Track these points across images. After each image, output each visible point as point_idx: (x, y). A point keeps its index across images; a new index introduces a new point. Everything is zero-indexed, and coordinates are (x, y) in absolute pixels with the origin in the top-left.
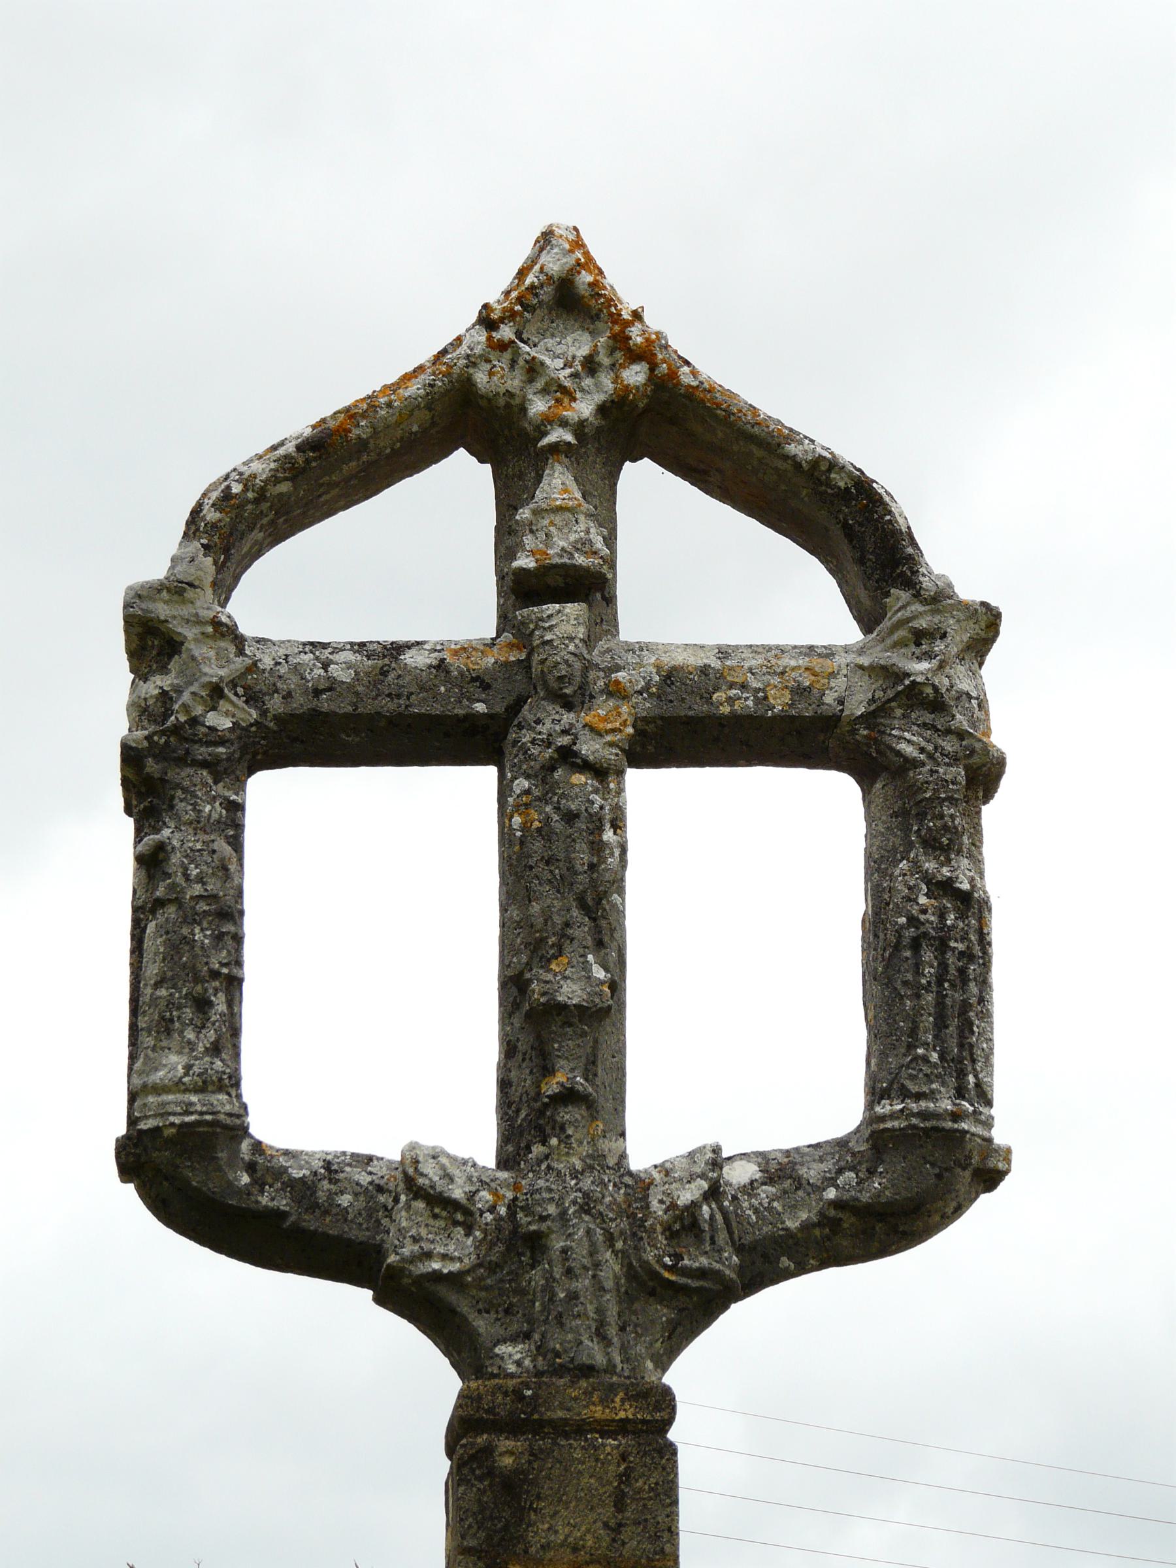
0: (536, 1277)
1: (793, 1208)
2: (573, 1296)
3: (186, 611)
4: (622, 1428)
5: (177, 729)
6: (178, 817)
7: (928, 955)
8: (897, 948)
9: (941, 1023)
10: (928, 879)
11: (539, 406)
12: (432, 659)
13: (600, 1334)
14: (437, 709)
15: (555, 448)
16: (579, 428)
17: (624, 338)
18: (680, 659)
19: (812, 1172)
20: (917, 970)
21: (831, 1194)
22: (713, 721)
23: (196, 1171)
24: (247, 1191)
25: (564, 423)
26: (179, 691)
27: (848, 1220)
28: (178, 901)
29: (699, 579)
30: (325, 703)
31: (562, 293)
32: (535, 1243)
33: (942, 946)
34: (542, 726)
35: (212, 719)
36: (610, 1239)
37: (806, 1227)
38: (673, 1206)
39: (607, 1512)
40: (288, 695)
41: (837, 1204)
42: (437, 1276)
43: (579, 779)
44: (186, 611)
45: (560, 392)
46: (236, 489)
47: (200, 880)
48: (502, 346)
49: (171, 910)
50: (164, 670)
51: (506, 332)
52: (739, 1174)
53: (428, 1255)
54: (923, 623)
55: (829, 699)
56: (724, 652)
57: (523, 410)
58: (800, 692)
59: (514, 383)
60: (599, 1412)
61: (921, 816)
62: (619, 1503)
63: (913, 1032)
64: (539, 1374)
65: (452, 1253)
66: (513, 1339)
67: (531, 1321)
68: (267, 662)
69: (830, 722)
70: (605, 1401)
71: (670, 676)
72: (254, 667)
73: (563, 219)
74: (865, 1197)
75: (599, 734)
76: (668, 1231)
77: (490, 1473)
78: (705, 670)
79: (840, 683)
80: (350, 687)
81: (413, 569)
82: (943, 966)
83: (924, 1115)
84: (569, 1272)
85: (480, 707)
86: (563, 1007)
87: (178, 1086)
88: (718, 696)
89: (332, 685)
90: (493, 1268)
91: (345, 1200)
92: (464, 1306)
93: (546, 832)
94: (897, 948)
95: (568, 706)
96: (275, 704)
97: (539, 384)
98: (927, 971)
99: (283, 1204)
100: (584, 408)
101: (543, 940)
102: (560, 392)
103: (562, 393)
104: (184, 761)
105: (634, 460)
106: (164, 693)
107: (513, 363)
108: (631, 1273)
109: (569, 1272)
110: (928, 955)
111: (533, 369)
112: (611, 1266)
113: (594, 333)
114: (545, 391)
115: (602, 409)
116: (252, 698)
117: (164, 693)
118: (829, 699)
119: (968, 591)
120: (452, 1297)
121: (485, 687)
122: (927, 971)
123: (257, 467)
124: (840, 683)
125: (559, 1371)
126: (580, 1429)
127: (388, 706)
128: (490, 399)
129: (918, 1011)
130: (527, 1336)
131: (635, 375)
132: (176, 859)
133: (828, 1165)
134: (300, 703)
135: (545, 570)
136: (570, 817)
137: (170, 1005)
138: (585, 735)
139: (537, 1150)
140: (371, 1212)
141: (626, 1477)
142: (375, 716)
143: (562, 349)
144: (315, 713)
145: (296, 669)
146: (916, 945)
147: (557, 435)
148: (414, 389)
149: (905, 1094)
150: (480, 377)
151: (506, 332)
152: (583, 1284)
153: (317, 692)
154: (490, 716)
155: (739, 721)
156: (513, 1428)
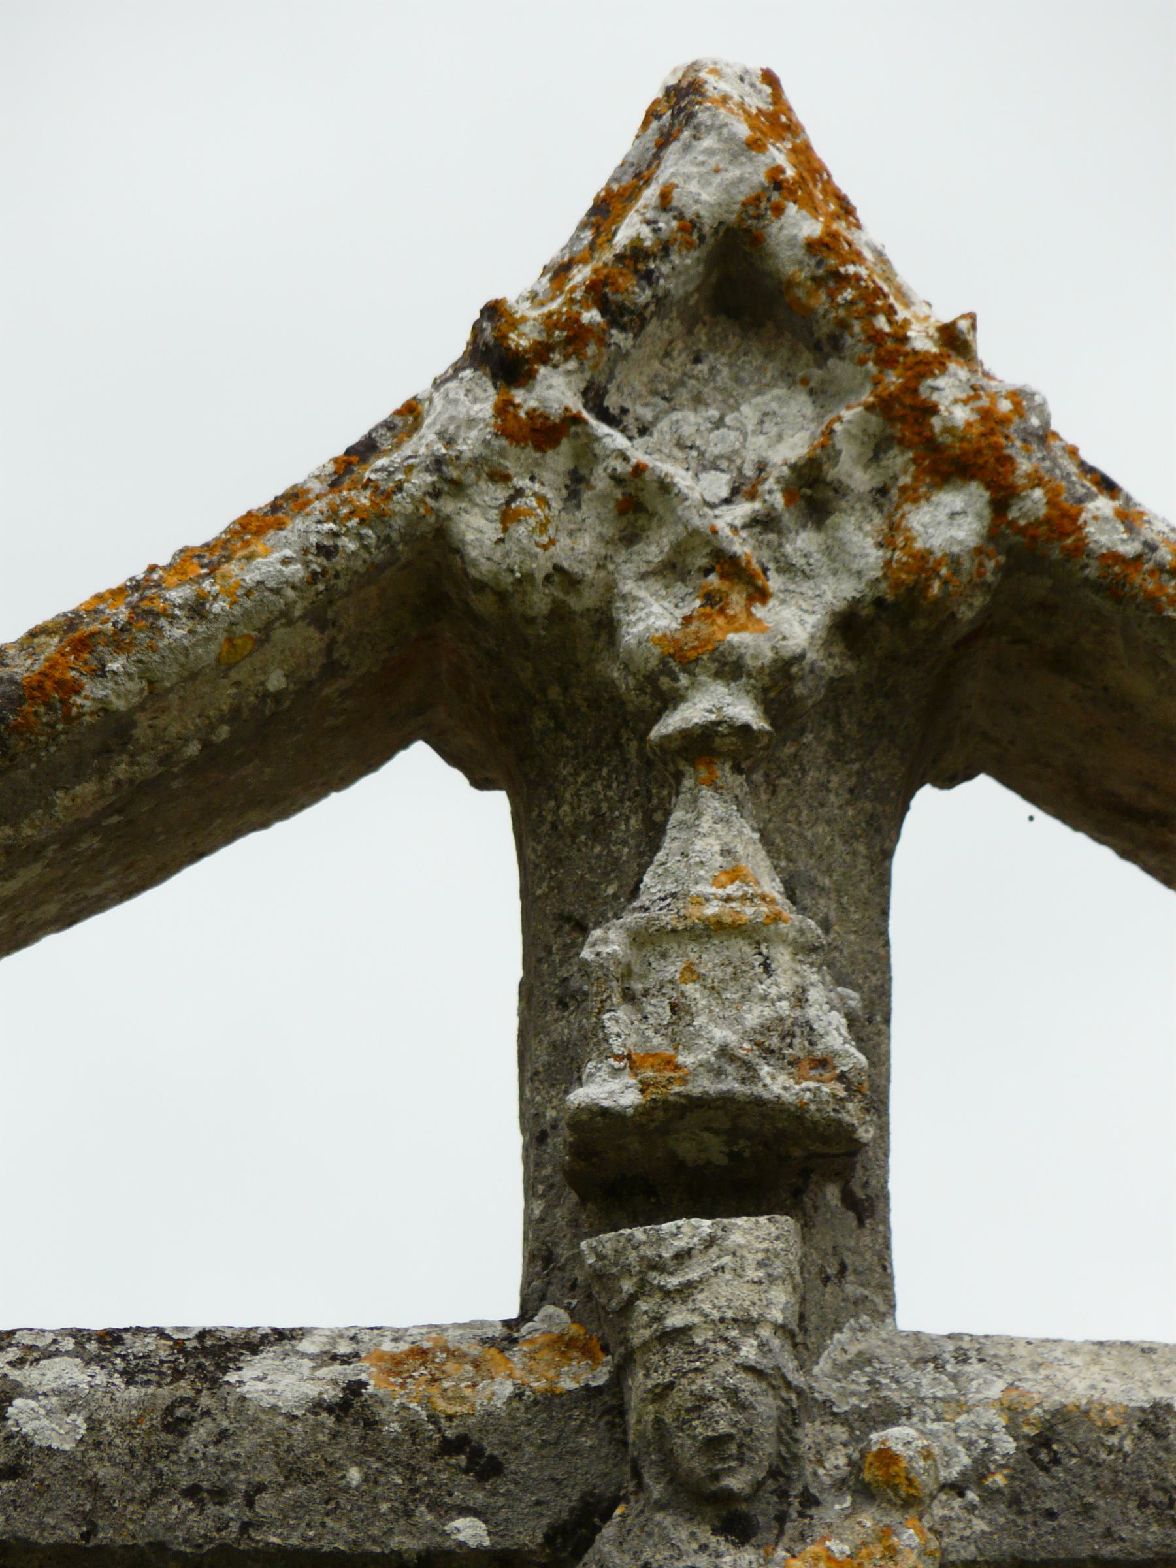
11: (653, 615)
12: (324, 1384)
14: (338, 1536)
15: (702, 744)
16: (778, 683)
17: (917, 409)
18: (1078, 1386)
25: (730, 668)
31: (733, 262)
48: (544, 432)
51: (556, 390)
57: (606, 625)
59: (579, 543)
71: (1050, 1439)
85: (469, 1531)
97: (654, 550)
100: (792, 623)
103: (729, 577)
107: (576, 485)
111: (638, 503)
113: (823, 395)
114: (672, 570)
121: (486, 1468)
127: (185, 1523)
128: (505, 594)
131: (948, 522)
135: (668, 1114)
148: (274, 561)
150: (476, 527)
151: (556, 390)
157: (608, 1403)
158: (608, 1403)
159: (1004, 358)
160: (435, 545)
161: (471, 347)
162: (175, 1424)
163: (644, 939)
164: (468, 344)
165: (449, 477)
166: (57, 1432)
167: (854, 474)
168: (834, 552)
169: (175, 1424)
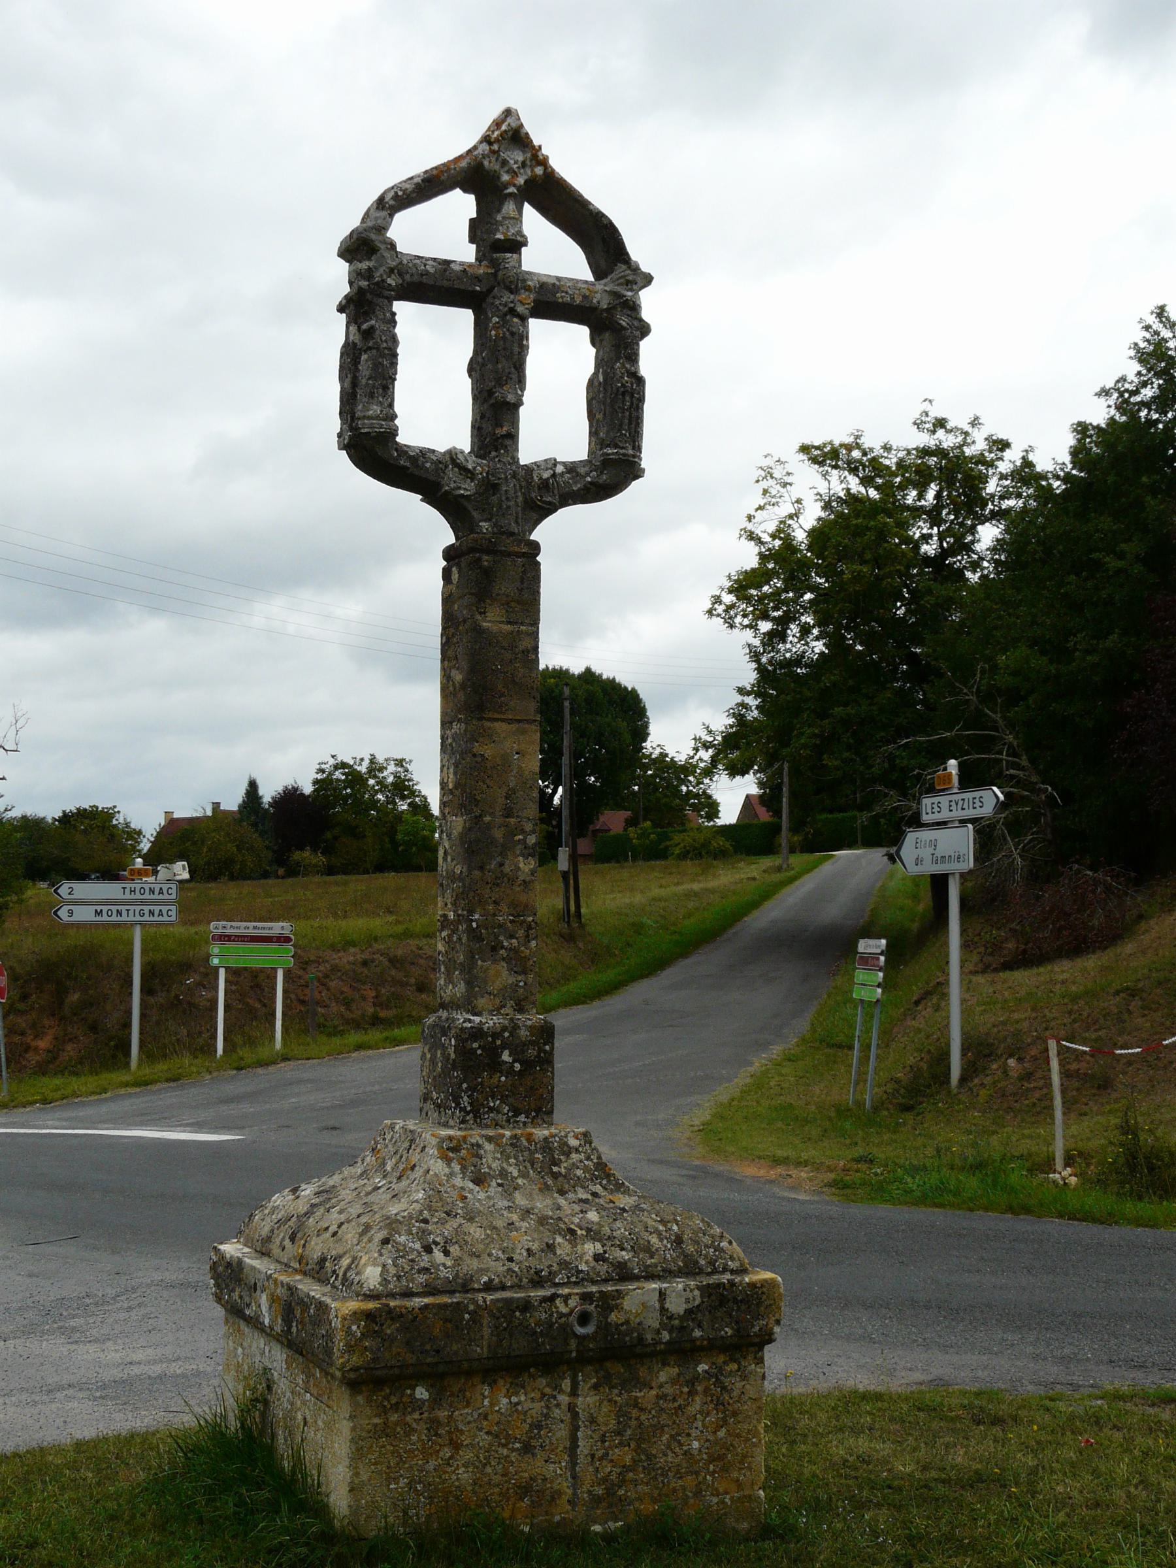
0: (494, 499)
1: (576, 483)
2: (509, 507)
3: (380, 238)
4: (523, 555)
5: (377, 283)
6: (376, 316)
7: (628, 398)
8: (616, 394)
9: (630, 423)
10: (627, 371)
11: (505, 177)
12: (461, 268)
13: (517, 522)
14: (462, 287)
15: (511, 194)
16: (519, 188)
17: (537, 158)
18: (545, 279)
19: (582, 471)
20: (624, 401)
21: (589, 479)
22: (555, 302)
23: (372, 446)
24: (396, 459)
25: (514, 185)
26: (376, 268)
27: (593, 488)
28: (378, 349)
29: (550, 253)
30: (424, 279)
31: (510, 135)
32: (495, 487)
33: (632, 396)
34: (495, 298)
35: (389, 281)
36: (521, 487)
37: (579, 490)
38: (541, 478)
39: (518, 584)
40: (412, 275)
41: (591, 483)
42: (462, 495)
43: (515, 320)
44: (380, 238)
45: (505, 173)
46: (400, 193)
47: (386, 341)
48: (493, 152)
49: (374, 352)
50: (369, 259)
51: (496, 147)
52: (560, 469)
53: (460, 488)
54: (630, 278)
55: (595, 301)
56: (559, 279)
57: (499, 178)
58: (585, 297)
59: (497, 167)
60: (516, 549)
61: (626, 348)
62: (522, 583)
63: (621, 425)
64: (494, 533)
65: (467, 488)
66: (485, 521)
67: (492, 514)
68: (405, 262)
69: (594, 309)
70: (518, 546)
71: (543, 285)
72: (401, 263)
73: (513, 106)
74: (601, 481)
75: (524, 304)
76: (539, 488)
77: (480, 567)
78: (554, 285)
79: (598, 296)
80: (433, 275)
81: (440, 231)
82: (632, 403)
83: (624, 455)
84: (507, 499)
85: (478, 288)
86: (508, 403)
87: (377, 418)
88: (558, 295)
89: (427, 273)
90: (480, 495)
91: (428, 465)
92: (470, 508)
93: (504, 338)
94: (616, 394)
95: (512, 293)
96: (407, 277)
97: (506, 169)
98: (617, 402)
99: (408, 464)
100: (521, 181)
101: (501, 378)
102: (505, 173)
103: (512, 172)
104: (379, 295)
105: (465, 191)
106: (369, 268)
107: (497, 159)
108: (525, 501)
109: (507, 499)
110: (628, 398)
111: (504, 163)
112: (520, 499)
113: (524, 152)
114: (507, 172)
115: (526, 182)
116: (400, 274)
117: (369, 268)
118: (595, 301)
119: (644, 268)
120: (466, 504)
121: (480, 281)
122: (617, 402)
123: (408, 186)
124: (598, 296)
125: (503, 533)
126: (509, 554)
127: (446, 283)
128: (488, 172)
129: (623, 417)
130: (490, 520)
131: (539, 171)
132: (378, 332)
133: (587, 469)
134: (416, 278)
135: (507, 240)
136: (513, 334)
137: (374, 386)
138: (518, 304)
139: (493, 454)
140: (437, 470)
141: (524, 572)
142: (435, 285)
143: (516, 157)
144: (421, 283)
145: (415, 265)
146: (623, 394)
147: (512, 190)
148: (464, 164)
149: (616, 446)
150: (486, 163)
151: (496, 147)
152: (512, 503)
153: (422, 275)
154: (480, 292)
155: (564, 305)
156: (488, 552)
157: (495, 275)
158: (495, 275)
159: (544, 151)
160: (481, 165)
161: (523, 135)
162: (445, 270)
163: (503, 218)
164: (527, 134)
165: (484, 156)
166: (432, 271)
167: (528, 163)
168: (525, 173)
169: (445, 270)
